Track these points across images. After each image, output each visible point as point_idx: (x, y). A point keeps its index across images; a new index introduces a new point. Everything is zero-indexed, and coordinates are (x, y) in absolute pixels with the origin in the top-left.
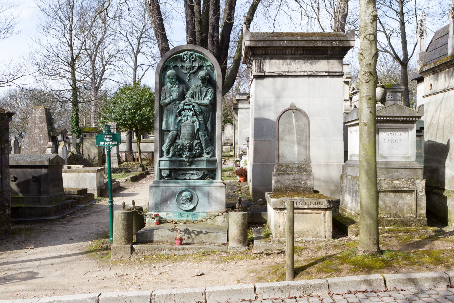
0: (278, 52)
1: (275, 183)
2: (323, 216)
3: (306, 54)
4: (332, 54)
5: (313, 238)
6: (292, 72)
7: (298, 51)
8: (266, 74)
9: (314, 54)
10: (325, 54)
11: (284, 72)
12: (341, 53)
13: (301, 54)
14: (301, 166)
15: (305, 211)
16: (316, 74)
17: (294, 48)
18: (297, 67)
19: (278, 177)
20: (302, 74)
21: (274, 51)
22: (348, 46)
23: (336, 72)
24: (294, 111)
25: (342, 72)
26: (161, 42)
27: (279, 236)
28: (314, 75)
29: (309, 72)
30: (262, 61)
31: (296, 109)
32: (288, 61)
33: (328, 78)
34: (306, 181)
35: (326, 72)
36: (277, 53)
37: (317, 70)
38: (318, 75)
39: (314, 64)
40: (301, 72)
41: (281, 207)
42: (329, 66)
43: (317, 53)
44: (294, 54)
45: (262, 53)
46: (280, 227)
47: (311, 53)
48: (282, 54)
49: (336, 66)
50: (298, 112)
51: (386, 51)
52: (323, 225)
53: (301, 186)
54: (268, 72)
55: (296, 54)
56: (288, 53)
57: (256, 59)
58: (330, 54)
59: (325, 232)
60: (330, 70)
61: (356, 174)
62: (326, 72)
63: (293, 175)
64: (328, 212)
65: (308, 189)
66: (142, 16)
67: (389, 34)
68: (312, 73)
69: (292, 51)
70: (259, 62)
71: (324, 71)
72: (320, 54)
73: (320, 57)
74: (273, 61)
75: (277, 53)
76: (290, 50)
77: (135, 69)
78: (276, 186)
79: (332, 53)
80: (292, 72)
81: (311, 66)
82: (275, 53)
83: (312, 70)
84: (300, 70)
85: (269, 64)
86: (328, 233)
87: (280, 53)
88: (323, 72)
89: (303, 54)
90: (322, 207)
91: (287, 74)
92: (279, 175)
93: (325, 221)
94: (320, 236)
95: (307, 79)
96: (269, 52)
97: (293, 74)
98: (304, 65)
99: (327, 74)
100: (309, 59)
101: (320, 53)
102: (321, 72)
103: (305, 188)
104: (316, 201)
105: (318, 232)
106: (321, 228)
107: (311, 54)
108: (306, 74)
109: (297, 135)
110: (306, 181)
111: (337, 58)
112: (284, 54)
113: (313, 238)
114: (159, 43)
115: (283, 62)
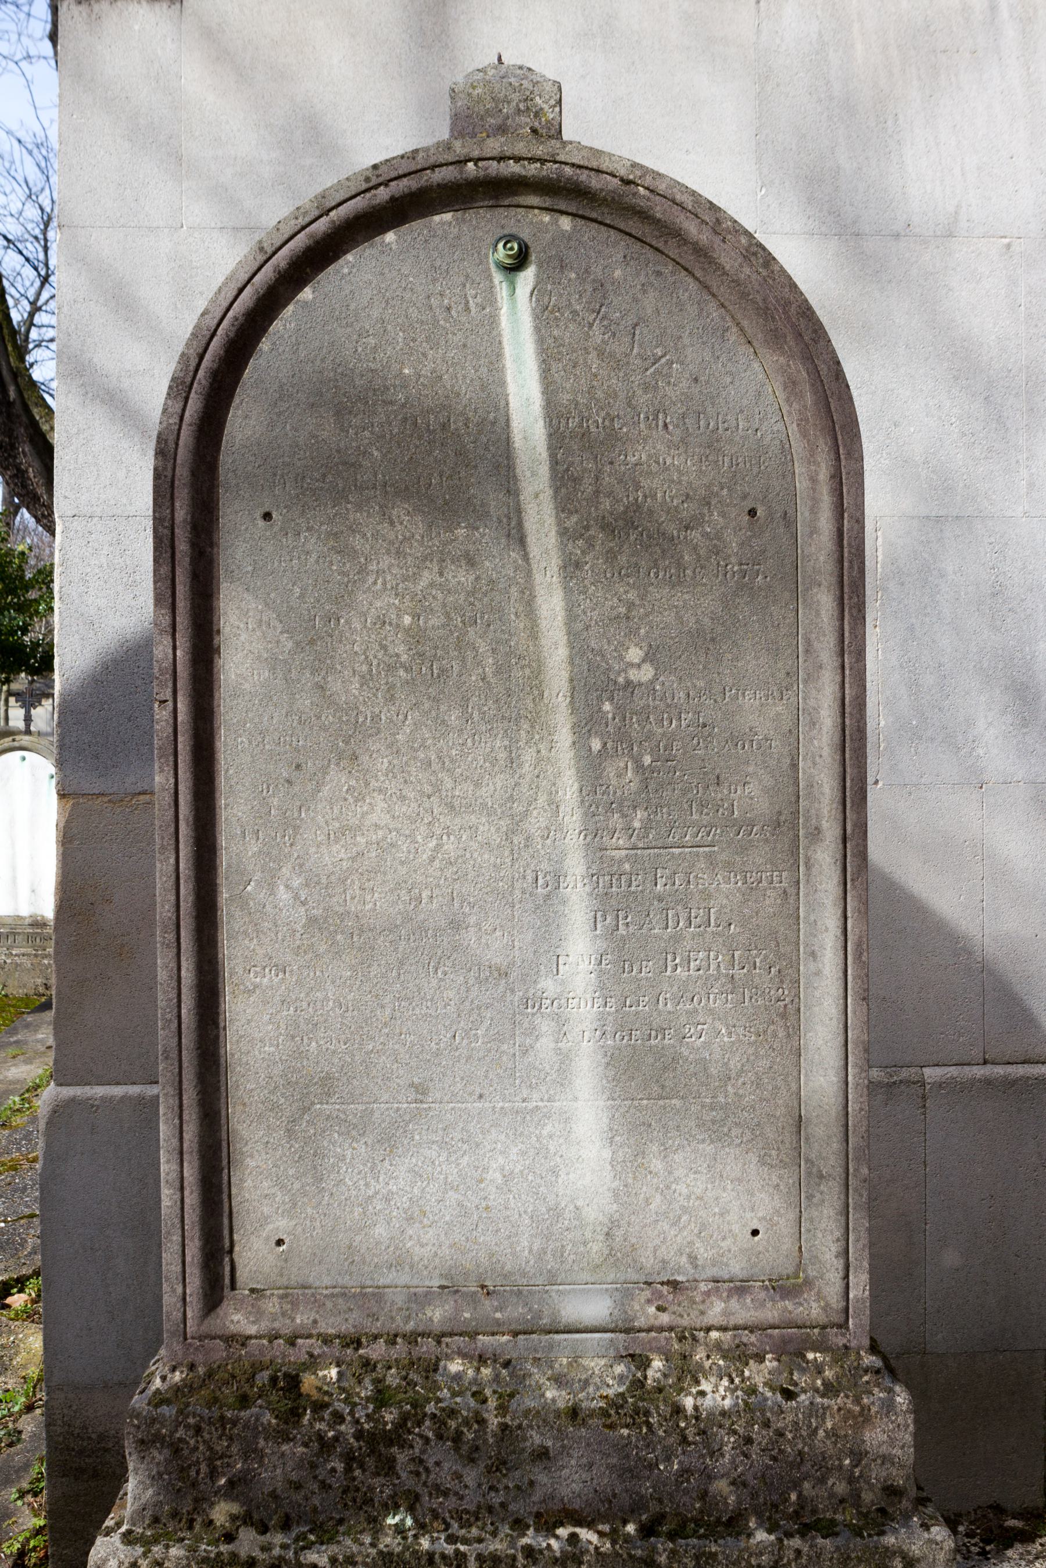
66: (36, 238)
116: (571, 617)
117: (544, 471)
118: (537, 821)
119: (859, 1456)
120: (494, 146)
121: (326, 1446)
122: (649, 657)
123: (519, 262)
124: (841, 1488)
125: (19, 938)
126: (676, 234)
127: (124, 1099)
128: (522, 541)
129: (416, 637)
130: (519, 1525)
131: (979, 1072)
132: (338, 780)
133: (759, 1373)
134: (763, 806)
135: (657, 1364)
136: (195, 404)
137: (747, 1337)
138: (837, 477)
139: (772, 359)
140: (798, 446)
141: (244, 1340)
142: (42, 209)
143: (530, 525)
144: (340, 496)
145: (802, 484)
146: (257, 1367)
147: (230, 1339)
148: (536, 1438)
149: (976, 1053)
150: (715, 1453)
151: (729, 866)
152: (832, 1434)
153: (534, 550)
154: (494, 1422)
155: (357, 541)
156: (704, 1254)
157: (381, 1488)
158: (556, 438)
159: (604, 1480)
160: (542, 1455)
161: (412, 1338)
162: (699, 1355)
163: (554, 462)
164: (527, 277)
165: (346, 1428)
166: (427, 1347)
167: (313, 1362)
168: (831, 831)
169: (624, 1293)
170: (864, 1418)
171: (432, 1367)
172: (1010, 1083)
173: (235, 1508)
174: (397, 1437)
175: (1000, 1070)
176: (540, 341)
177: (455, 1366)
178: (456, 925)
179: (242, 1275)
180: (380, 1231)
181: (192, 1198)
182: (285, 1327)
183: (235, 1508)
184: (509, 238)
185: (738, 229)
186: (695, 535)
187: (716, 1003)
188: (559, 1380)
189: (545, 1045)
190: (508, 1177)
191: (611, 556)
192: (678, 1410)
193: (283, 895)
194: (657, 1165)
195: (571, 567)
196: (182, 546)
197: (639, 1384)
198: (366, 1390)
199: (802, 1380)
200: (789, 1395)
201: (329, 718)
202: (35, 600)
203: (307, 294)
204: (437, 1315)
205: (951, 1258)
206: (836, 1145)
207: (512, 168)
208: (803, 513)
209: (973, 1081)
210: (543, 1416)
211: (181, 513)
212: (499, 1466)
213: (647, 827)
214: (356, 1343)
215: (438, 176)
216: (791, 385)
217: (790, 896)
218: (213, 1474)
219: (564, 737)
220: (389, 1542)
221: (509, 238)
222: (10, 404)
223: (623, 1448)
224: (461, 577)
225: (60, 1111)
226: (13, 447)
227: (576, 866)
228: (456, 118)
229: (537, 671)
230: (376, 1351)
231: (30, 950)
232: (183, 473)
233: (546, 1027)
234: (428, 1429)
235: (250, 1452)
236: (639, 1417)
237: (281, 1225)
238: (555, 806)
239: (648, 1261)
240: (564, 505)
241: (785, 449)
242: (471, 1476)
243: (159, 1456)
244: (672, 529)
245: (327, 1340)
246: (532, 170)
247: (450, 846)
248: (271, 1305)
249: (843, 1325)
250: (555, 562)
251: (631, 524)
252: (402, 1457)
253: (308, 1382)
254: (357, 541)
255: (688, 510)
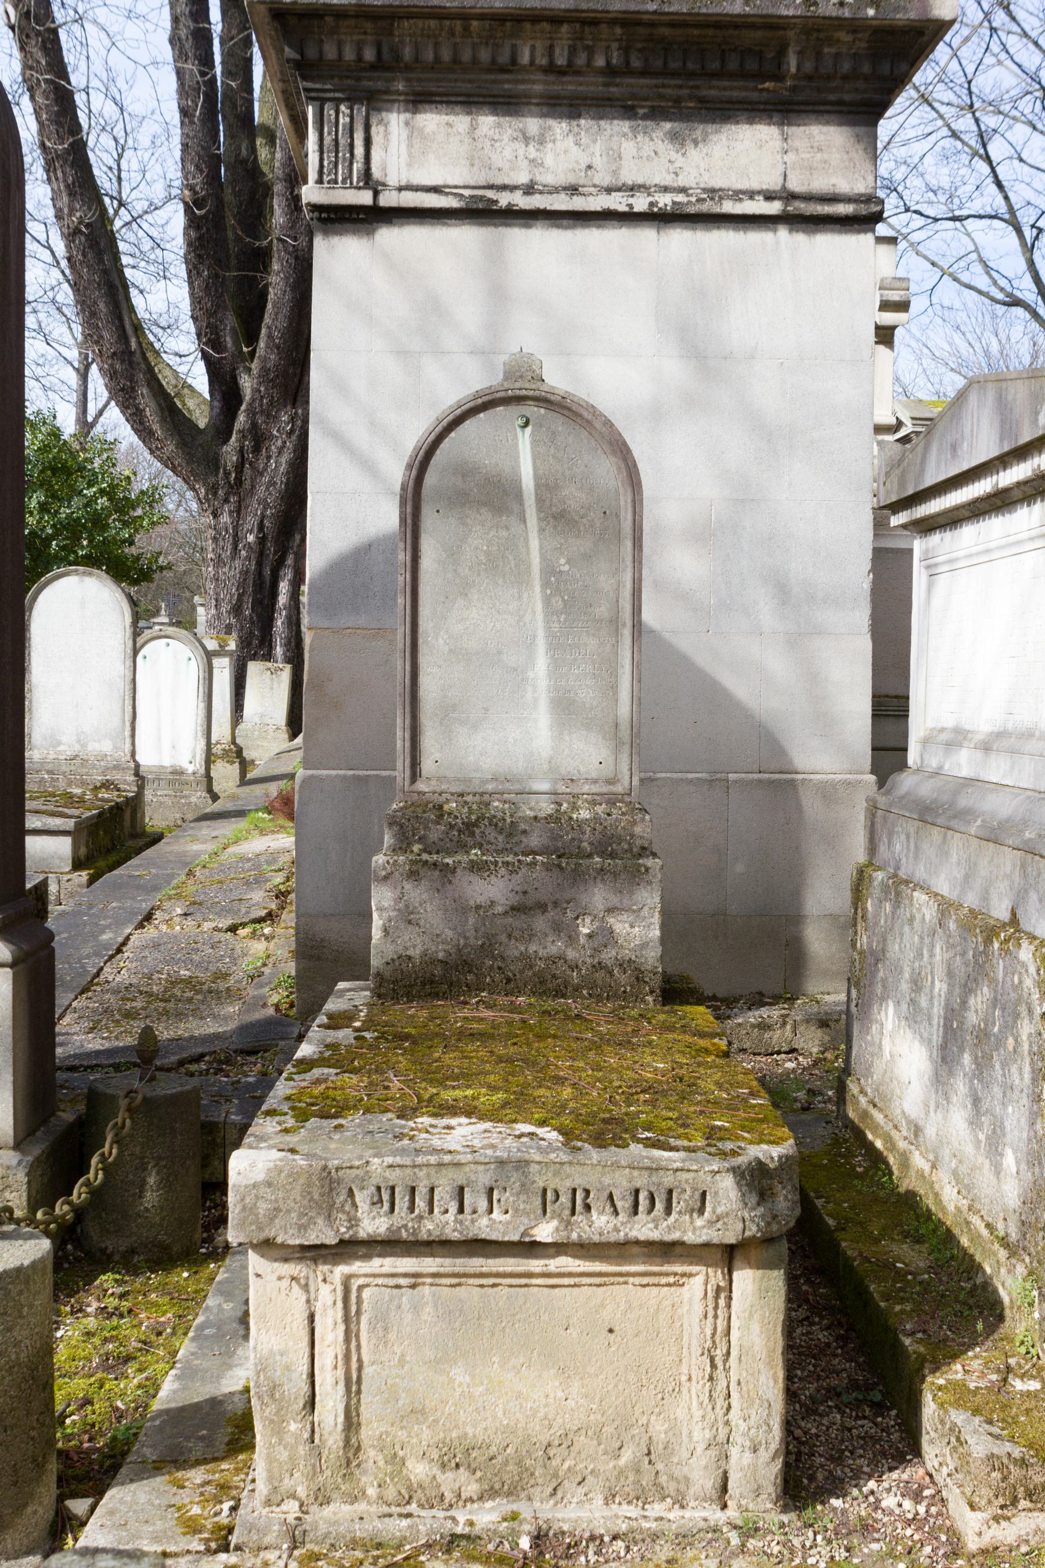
0: (466, 56)
1: (386, 931)
2: (698, 1309)
3: (644, 73)
4: (810, 78)
5: (610, 1498)
6: (555, 190)
7: (590, 51)
8: (387, 199)
9: (692, 75)
10: (763, 77)
11: (504, 188)
12: (866, 69)
13: (610, 71)
14: (574, 807)
15: (536, 1265)
16: (705, 208)
17: (565, 28)
18: (584, 162)
19: (408, 886)
20: (617, 202)
21: (436, 45)
22: (912, 15)
23: (833, 199)
24: (532, 410)
25: (869, 199)
26: (65, 199)
27: (301, 1492)
28: (691, 210)
29: (666, 189)
30: (361, 111)
31: (546, 401)
32: (533, 124)
33: (783, 233)
34: (611, 920)
35: (769, 197)
36: (456, 60)
37: (717, 183)
38: (717, 209)
39: (696, 143)
40: (609, 190)
41: (312, 1238)
42: (790, 157)
43: (715, 65)
44: (569, 70)
45: (360, 59)
46: (311, 1403)
47: (674, 65)
48: (489, 71)
49: (836, 157)
50: (558, 423)
51: (1015, 302)
52: (699, 1388)
53: (571, 954)
54: (400, 189)
55: (578, 73)
56: (525, 58)
57: (322, 101)
58: (795, 77)
59: (721, 1448)
60: (795, 185)
61: (985, 897)
62: (769, 197)
63: (518, 878)
64: (745, 1279)
65: (623, 979)
66: (110, 168)
67: (1033, 226)
68: (681, 198)
69: (551, 47)
70: (344, 120)
71: (755, 186)
72: (732, 76)
73: (735, 94)
74: (431, 121)
75: (456, 60)
76: (539, 45)
77: (82, 367)
78: (390, 951)
79: (808, 67)
80: (555, 190)
81: (673, 155)
82: (446, 55)
83: (681, 182)
84: (603, 178)
85: (404, 133)
86: (748, 1457)
87: (475, 61)
88: (751, 195)
89: (627, 71)
90: (690, 1238)
91: (522, 202)
92: (413, 875)
93: (719, 1353)
94: (671, 1488)
95: (647, 235)
96: (407, 53)
97: (561, 203)
98: (628, 147)
99: (774, 208)
100: (657, 114)
101: (733, 65)
102: (737, 195)
103: (600, 966)
104: (641, 1180)
105: (658, 1449)
106: (680, 1413)
107: (674, 74)
108: (641, 204)
109: (546, 584)
110: (611, 920)
111: (840, 103)
112: (503, 70)
113: (610, 1498)
114: (59, 204)
115: (499, 125)
116: (541, 548)
117: (533, 497)
118: (528, 618)
119: (632, 836)
120: (518, 385)
121: (452, 827)
122: (568, 562)
123: (526, 424)
124: (626, 847)
125: (162, 783)
126: (581, 416)
127: (337, 776)
128: (525, 522)
129: (488, 554)
130: (516, 854)
131: (756, 776)
132: (460, 602)
133: (600, 809)
134: (606, 615)
135: (565, 805)
136: (414, 472)
137: (596, 797)
138: (634, 501)
139: (613, 459)
140: (621, 490)
141: (424, 793)
142: (116, 140)
143: (528, 516)
144: (463, 505)
145: (622, 503)
146: (428, 802)
147: (419, 793)
148: (523, 826)
149: (755, 767)
150: (583, 833)
151: (594, 635)
152: (623, 828)
153: (529, 525)
154: (509, 820)
155: (468, 521)
156: (583, 769)
157: (470, 841)
158: (537, 486)
159: (545, 841)
160: (524, 832)
161: (482, 794)
162: (580, 803)
163: (537, 494)
164: (529, 429)
165: (459, 821)
166: (486, 797)
167: (448, 801)
168: (629, 623)
169: (555, 782)
170: (634, 823)
171: (487, 804)
172: (772, 782)
173: (421, 847)
174: (475, 824)
175: (767, 776)
176: (533, 452)
177: (496, 804)
178: (500, 653)
179: (423, 773)
180: (471, 758)
181: (408, 744)
182: (438, 789)
183: (421, 847)
184: (523, 416)
185: (602, 415)
186: (585, 520)
187: (588, 682)
188: (531, 809)
189: (529, 695)
190: (515, 741)
191: (555, 527)
192: (571, 818)
193: (441, 641)
194: (567, 738)
195: (541, 530)
196: (409, 521)
197: (558, 811)
198: (466, 810)
199: (614, 811)
200: (609, 815)
201: (457, 581)
202: (139, 517)
203: (453, 434)
204: (490, 787)
205: (740, 868)
206: (628, 732)
207: (524, 393)
208: (622, 513)
209: (753, 780)
210: (524, 819)
211: (409, 510)
212: (510, 835)
213: (566, 620)
214: (462, 795)
215: (499, 395)
216: (619, 469)
217: (616, 645)
218: (414, 835)
219: (538, 589)
220: (472, 857)
221: (523, 416)
222: (132, 354)
223: (552, 830)
224: (504, 533)
225: (306, 781)
226: (133, 389)
227: (541, 633)
228: (505, 373)
229: (529, 566)
230: (469, 798)
231: (171, 792)
232: (410, 496)
233: (529, 689)
234: (486, 821)
235: (426, 828)
236: (558, 820)
237: (437, 756)
238: (534, 612)
239: (563, 772)
240: (540, 509)
241: (617, 491)
242: (501, 838)
243: (396, 828)
244: (577, 518)
245: (452, 794)
246: (531, 393)
247: (498, 625)
248: (433, 783)
249: (629, 794)
250: (536, 529)
251: (562, 516)
252: (477, 831)
253: (446, 807)
254: (468, 521)
255: (582, 512)
